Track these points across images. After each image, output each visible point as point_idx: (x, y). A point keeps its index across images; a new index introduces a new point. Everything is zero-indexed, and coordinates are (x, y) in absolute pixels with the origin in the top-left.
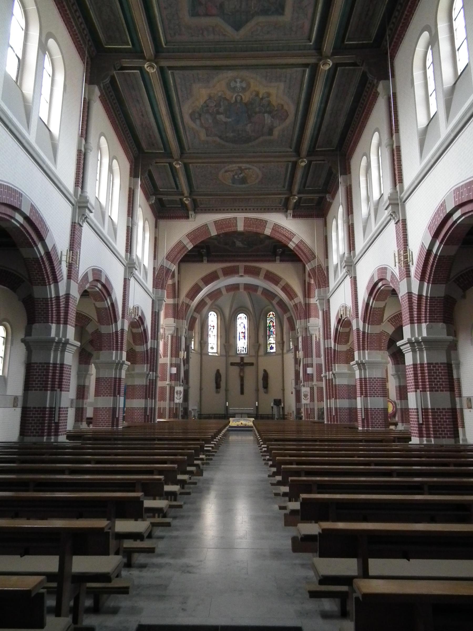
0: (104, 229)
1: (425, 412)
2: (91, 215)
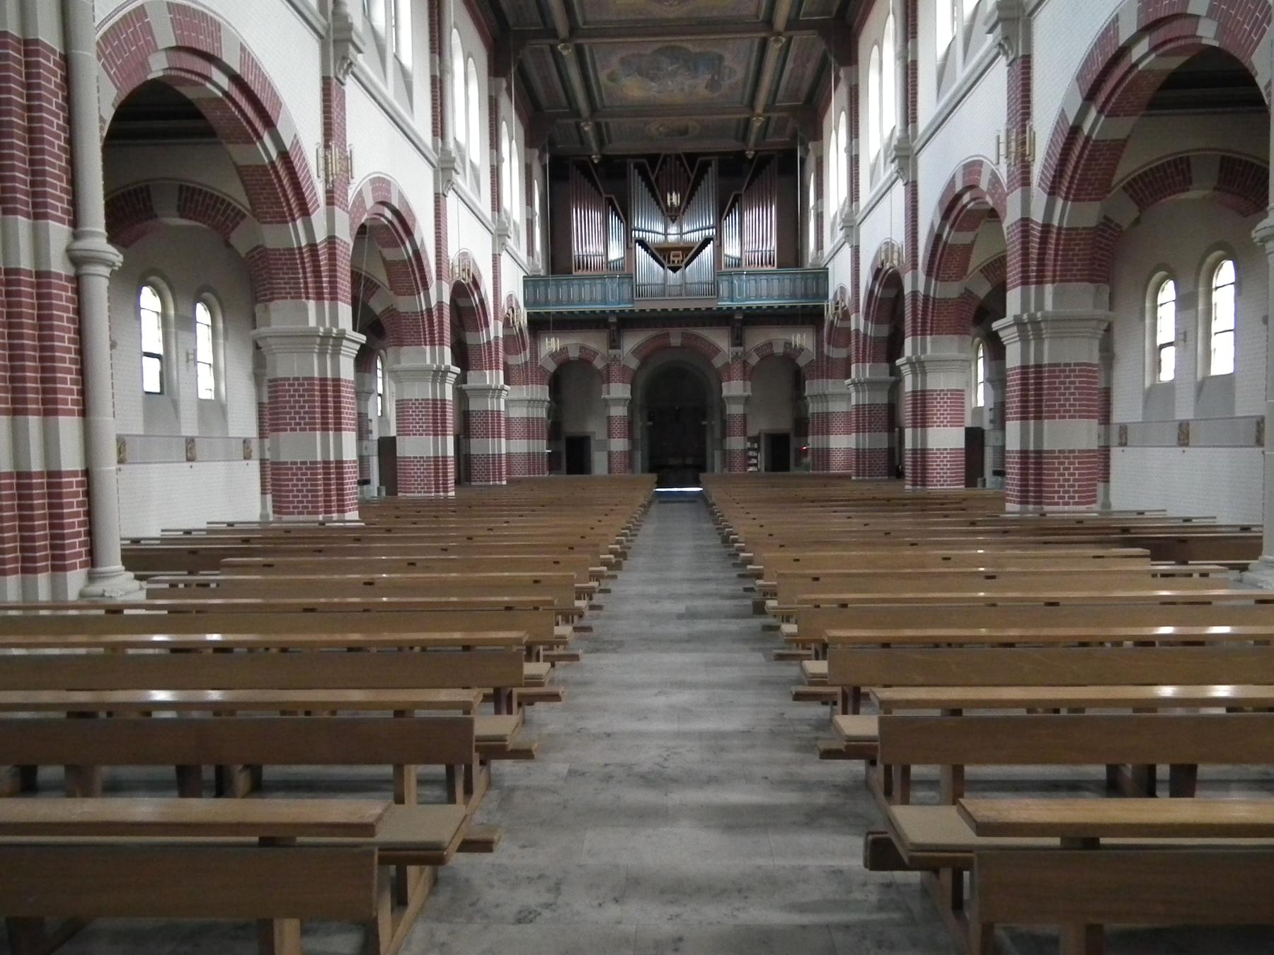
2: (360, 57)
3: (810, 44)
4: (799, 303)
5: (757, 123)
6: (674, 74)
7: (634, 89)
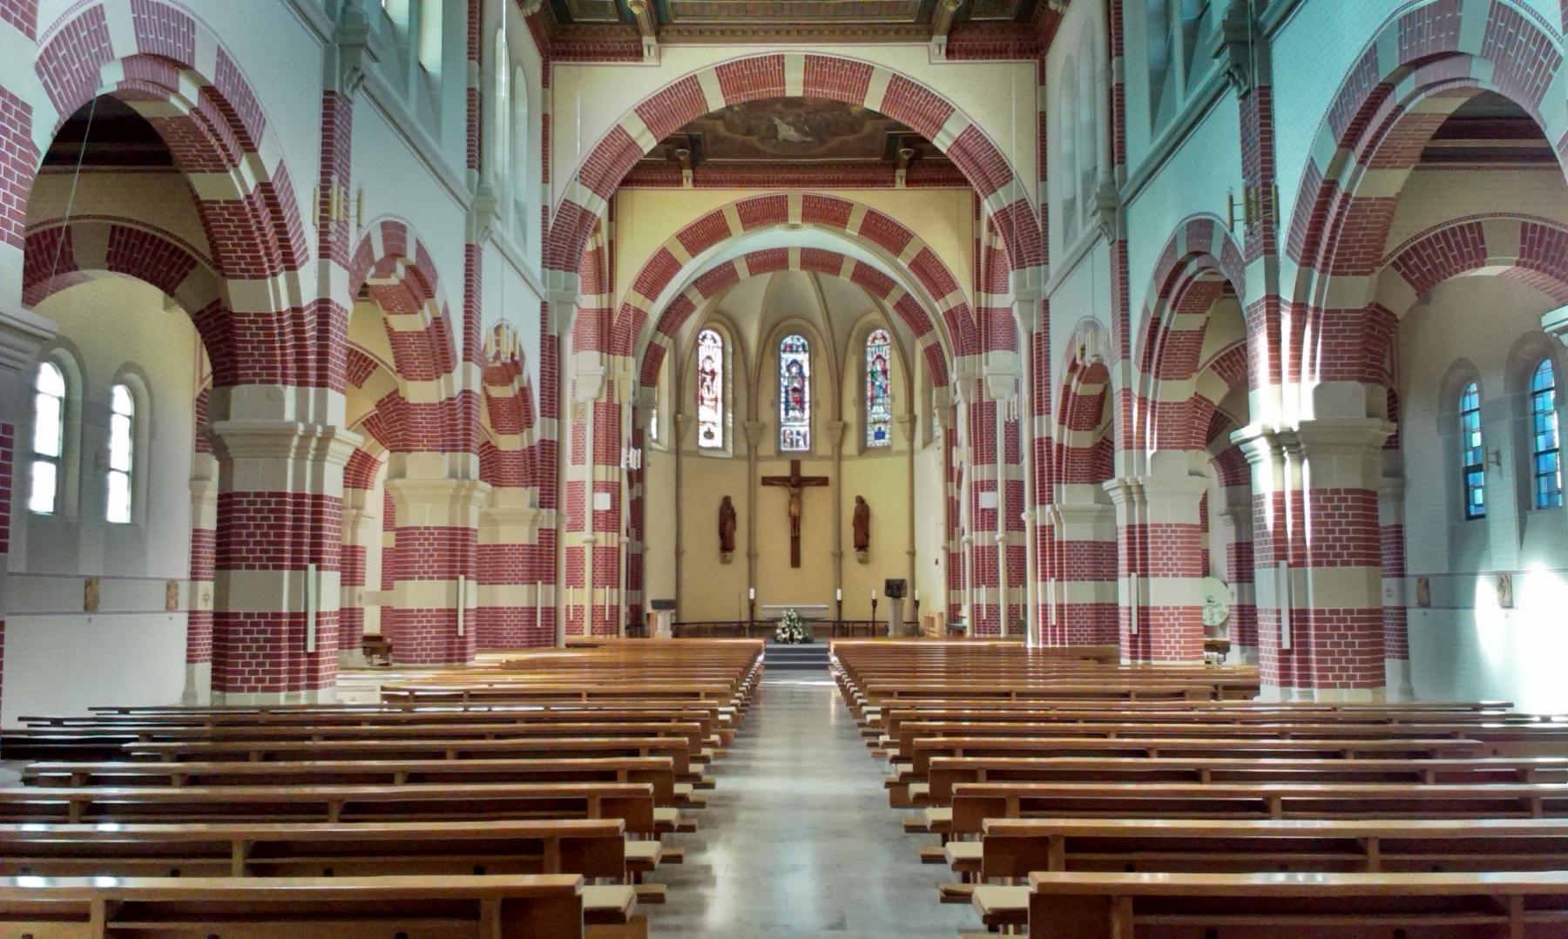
1: (1298, 620)
2: (375, 66)
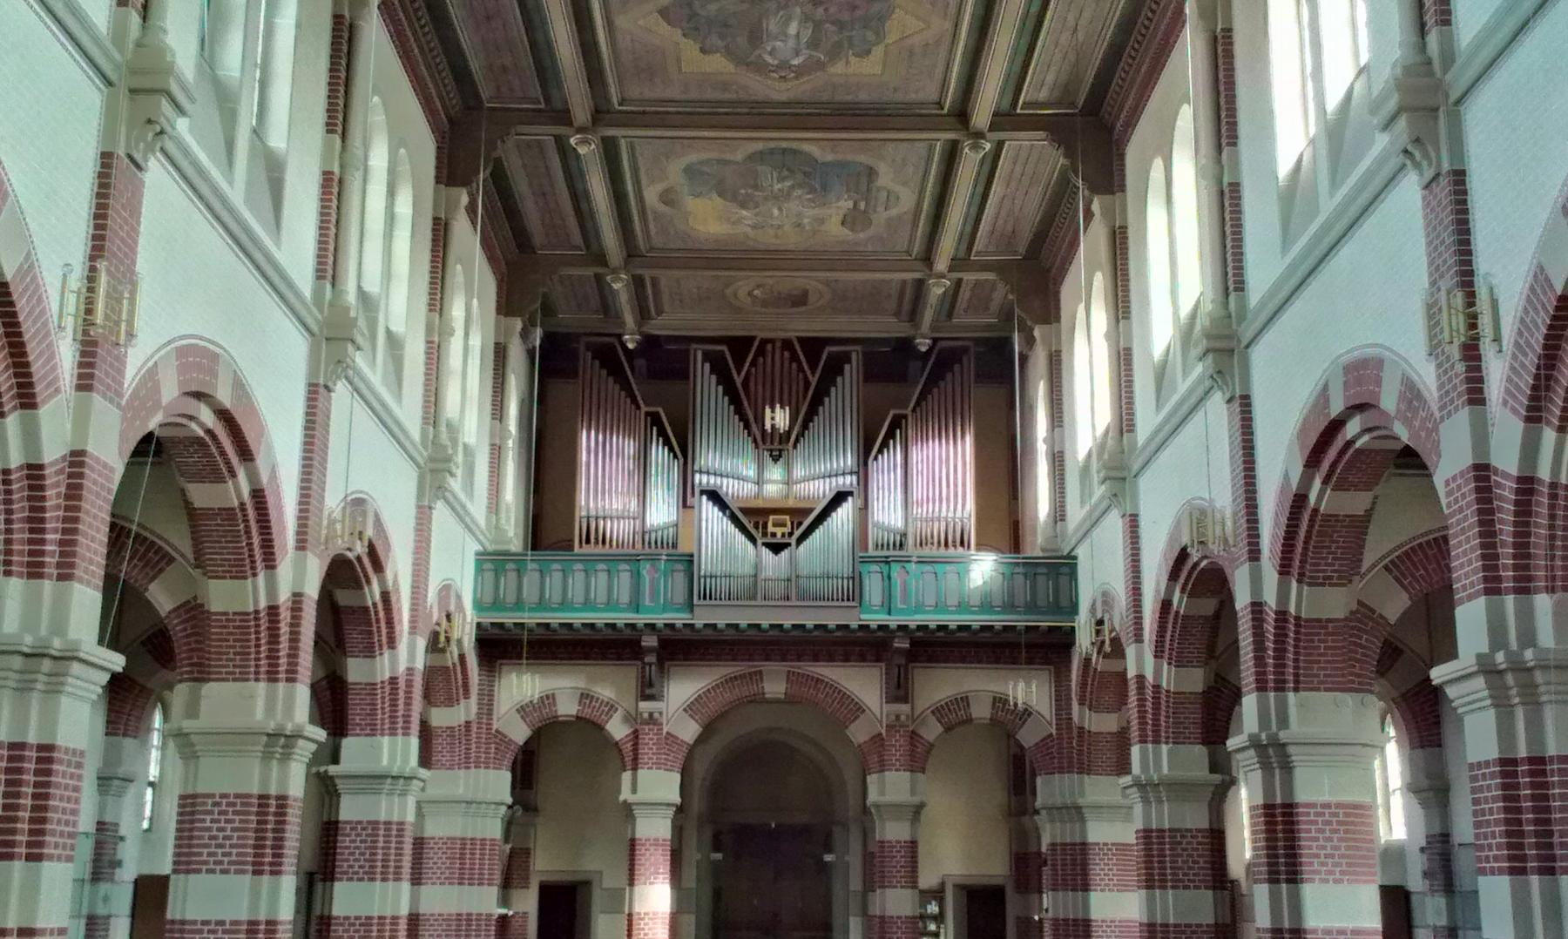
0: (231, 183)
2: (182, 125)
3: (1032, 160)
4: (1020, 621)
5: (936, 290)
6: (781, 198)
7: (709, 219)
